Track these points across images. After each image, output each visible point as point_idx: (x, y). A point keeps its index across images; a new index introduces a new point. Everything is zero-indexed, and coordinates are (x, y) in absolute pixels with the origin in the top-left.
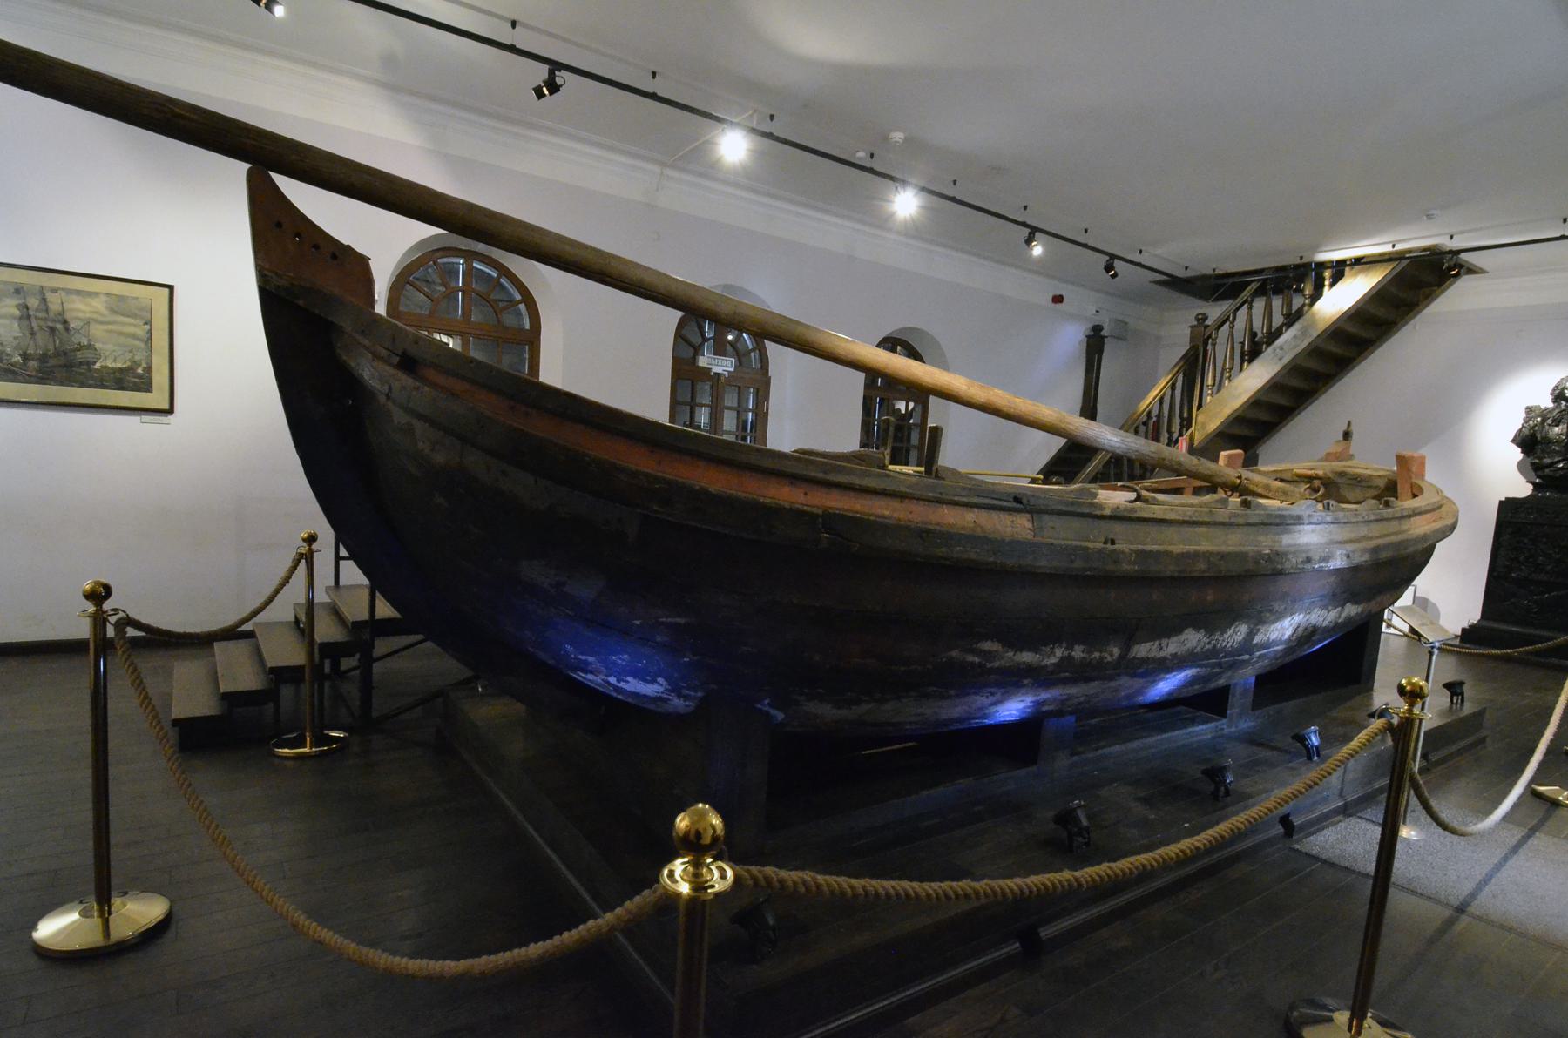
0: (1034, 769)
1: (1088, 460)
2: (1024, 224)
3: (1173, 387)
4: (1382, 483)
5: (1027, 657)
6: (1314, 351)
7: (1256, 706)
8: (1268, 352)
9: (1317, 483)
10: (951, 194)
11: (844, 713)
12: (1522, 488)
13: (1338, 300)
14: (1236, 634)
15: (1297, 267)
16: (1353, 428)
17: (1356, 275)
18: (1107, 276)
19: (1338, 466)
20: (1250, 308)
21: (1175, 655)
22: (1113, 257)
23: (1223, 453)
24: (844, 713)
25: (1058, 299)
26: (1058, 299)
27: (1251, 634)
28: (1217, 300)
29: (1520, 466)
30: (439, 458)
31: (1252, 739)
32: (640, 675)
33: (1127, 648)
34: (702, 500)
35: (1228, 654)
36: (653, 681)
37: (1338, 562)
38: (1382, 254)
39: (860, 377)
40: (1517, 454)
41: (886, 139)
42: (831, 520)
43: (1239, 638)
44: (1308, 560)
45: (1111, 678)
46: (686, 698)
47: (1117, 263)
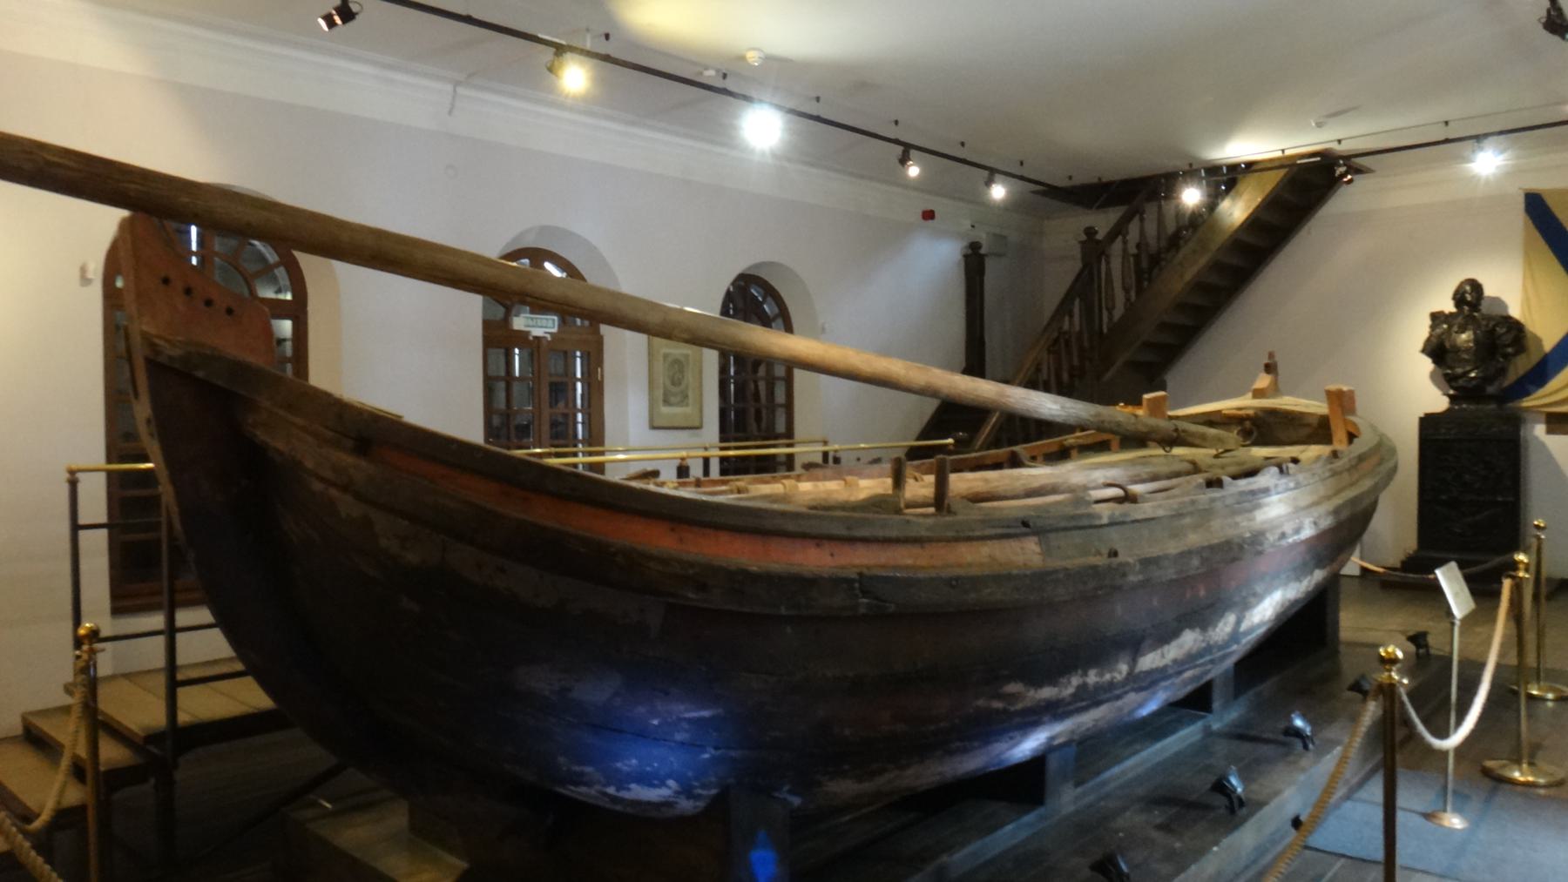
0: (1041, 811)
2: (897, 142)
4: (1315, 422)
5: (1047, 693)
6: (1216, 266)
7: (1237, 693)
11: (867, 786)
12: (1437, 401)
14: (1224, 627)
16: (1278, 358)
20: (1142, 220)
21: (1175, 661)
23: (1146, 396)
24: (867, 786)
25: (929, 215)
26: (929, 215)
27: (1239, 622)
29: (1433, 376)
30: (412, 557)
31: (1240, 734)
33: (1134, 662)
34: (740, 581)
35: (1221, 648)
36: (663, 784)
37: (1308, 532)
40: (1427, 364)
42: (865, 583)
43: (1228, 629)
44: (1283, 536)
45: (1118, 697)
46: (698, 797)
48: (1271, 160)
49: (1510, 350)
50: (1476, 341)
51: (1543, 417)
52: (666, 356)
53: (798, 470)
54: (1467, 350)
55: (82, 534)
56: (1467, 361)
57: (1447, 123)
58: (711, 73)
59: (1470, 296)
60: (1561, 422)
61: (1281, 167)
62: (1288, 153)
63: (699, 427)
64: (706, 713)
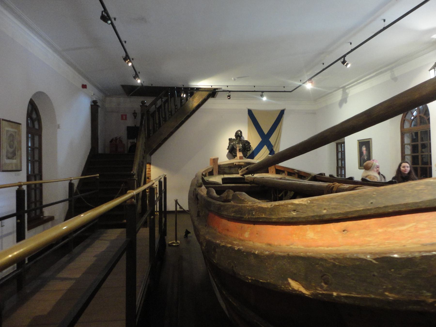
25: (84, 86)
26: (84, 86)
48: (205, 88)
52: (7, 131)
55: (174, 216)
57: (227, 86)
59: (239, 135)
61: (207, 91)
62: (213, 87)
63: (21, 170)
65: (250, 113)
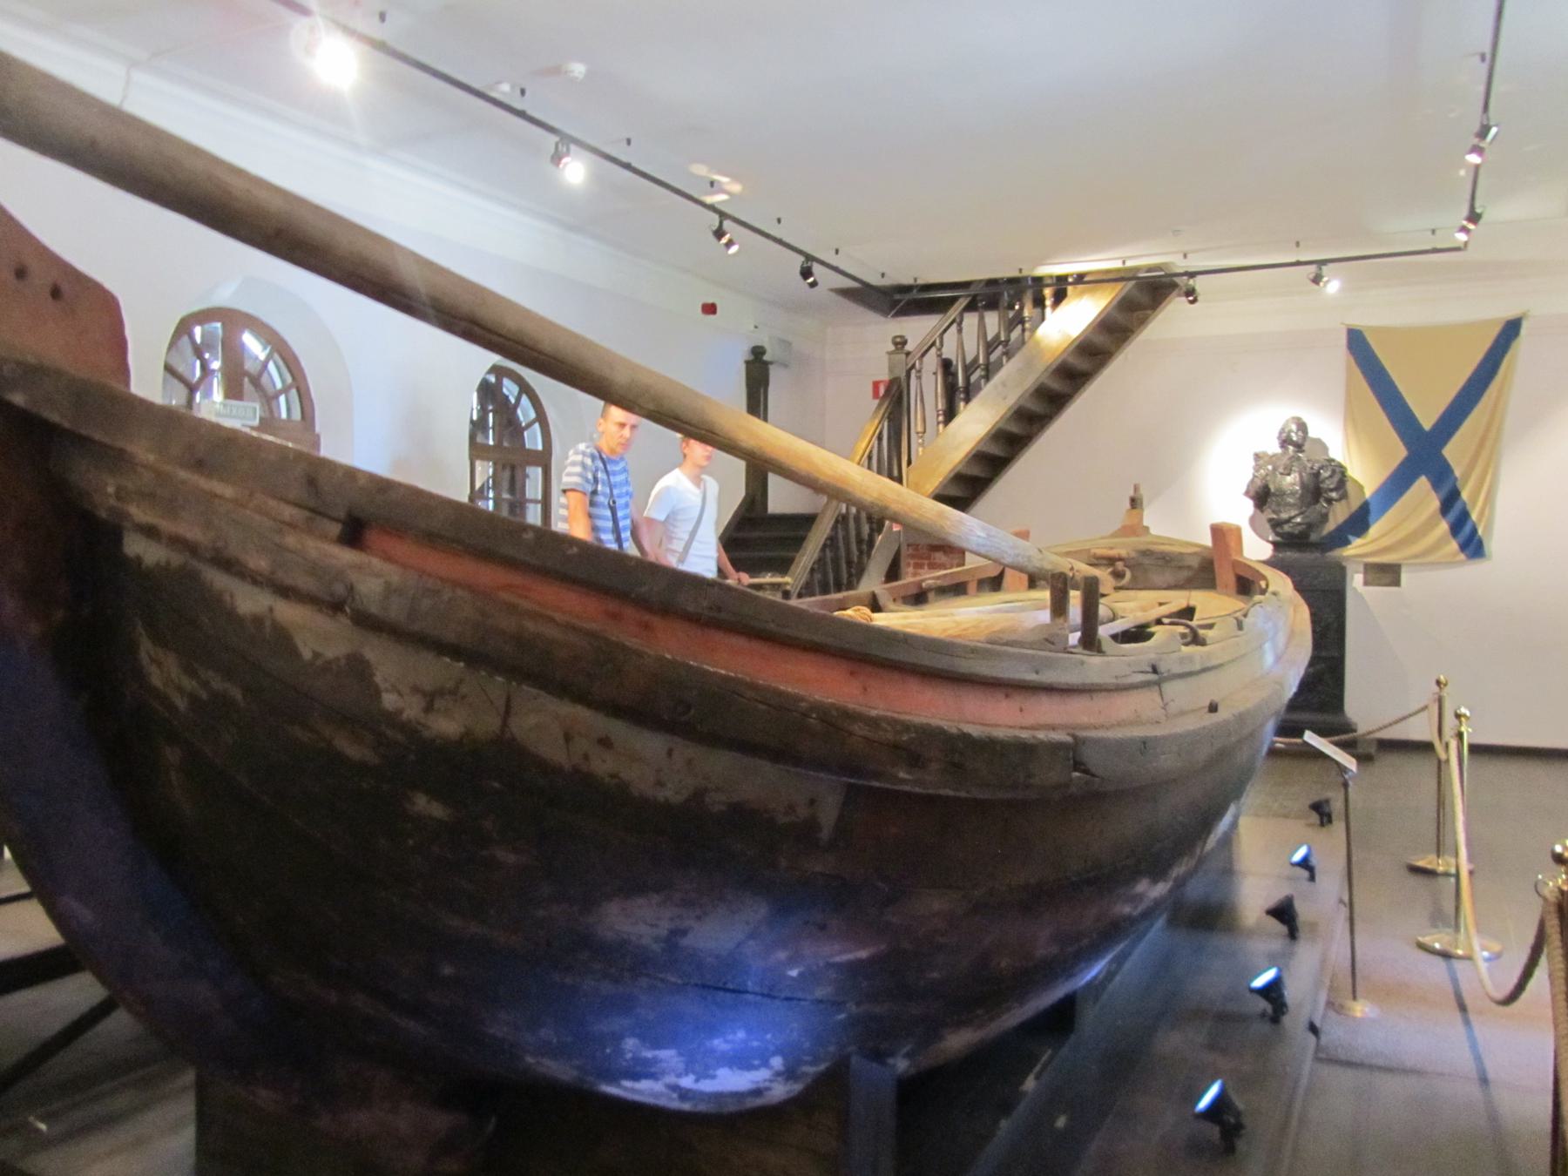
1: (798, 542)
3: (880, 438)
4: (1195, 562)
8: (988, 389)
9: (1120, 565)
10: (624, 159)
13: (1065, 324)
15: (1012, 281)
17: (1082, 293)
18: (803, 285)
19: (1134, 541)
20: (960, 331)
22: (809, 258)
25: (710, 309)
26: (710, 309)
28: (897, 314)
30: (447, 725)
32: (841, 953)
38: (1108, 271)
39: (741, 465)
41: (556, 71)
47: (816, 268)
49: (1334, 495)
50: (1303, 485)
51: (1361, 568)
53: (972, 587)
54: (1293, 494)
56: (1292, 505)
58: (505, 87)
59: (1296, 441)
60: (1386, 574)
62: (1130, 264)
64: (863, 954)
65: (1357, 343)
